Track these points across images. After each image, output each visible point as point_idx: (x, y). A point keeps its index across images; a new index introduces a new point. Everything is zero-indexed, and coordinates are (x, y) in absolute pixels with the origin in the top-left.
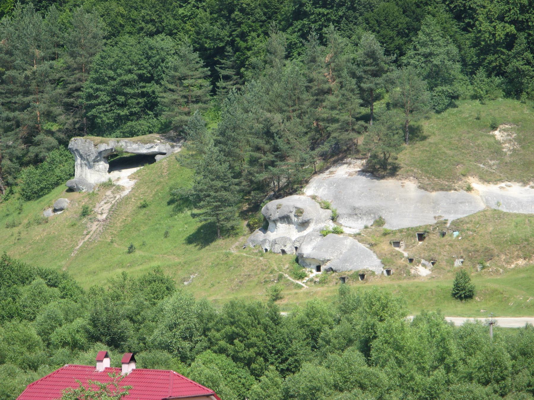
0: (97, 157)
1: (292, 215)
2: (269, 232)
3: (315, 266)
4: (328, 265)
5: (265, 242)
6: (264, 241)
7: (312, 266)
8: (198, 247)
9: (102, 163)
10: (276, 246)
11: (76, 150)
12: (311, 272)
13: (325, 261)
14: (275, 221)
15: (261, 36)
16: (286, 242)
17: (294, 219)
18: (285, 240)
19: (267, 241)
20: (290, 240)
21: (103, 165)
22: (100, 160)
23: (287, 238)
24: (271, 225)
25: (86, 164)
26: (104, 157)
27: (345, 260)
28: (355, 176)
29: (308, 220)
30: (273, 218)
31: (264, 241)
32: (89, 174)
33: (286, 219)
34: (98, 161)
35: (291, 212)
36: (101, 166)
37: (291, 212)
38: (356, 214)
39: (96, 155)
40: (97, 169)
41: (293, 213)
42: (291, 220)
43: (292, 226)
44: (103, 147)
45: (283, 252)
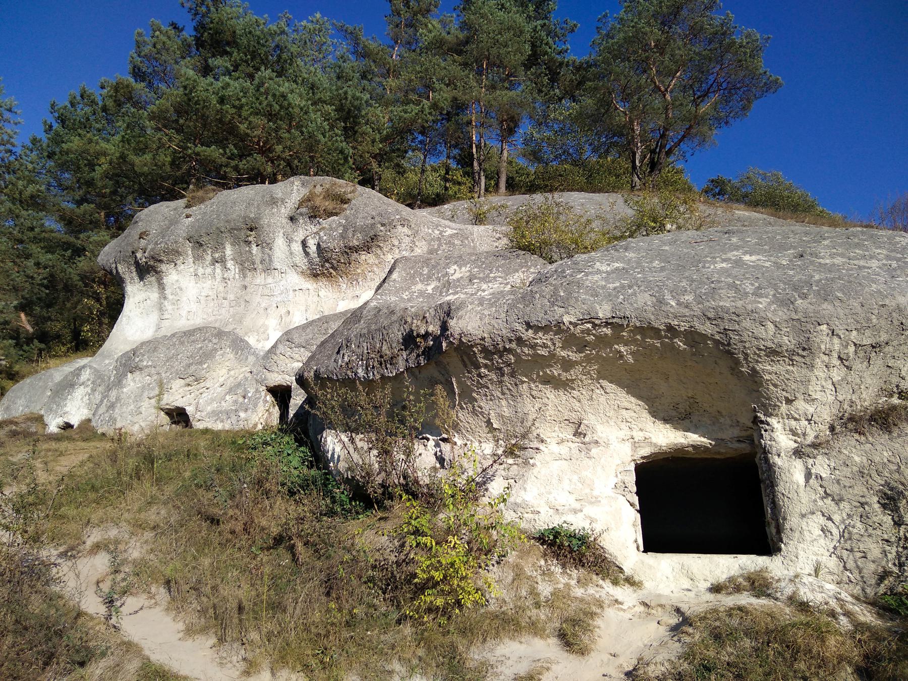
20: (239, 345)
23: (220, 334)
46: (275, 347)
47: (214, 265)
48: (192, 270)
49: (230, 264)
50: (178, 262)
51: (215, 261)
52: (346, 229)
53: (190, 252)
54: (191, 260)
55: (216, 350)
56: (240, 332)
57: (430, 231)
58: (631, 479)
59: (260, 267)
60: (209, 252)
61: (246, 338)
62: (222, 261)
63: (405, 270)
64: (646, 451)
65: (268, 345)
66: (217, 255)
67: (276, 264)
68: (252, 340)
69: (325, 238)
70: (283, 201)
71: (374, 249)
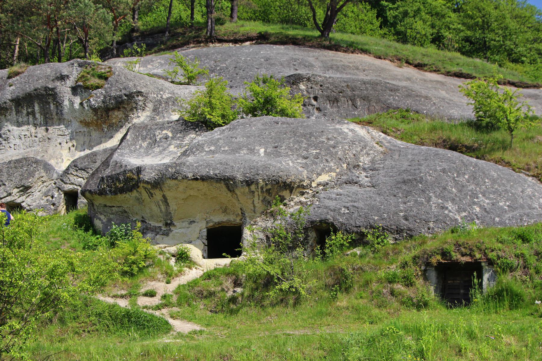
3: (200, 228)
12: (182, 257)
13: (280, 188)
16: (31, 174)
17: (71, 102)
20: (48, 168)
23: (37, 162)
29: (130, 96)
41: (70, 83)
42: (59, 105)
46: (68, 169)
47: (28, 116)
48: (15, 119)
49: (38, 115)
50: (7, 114)
51: (28, 114)
52: (105, 97)
53: (14, 108)
54: (14, 113)
55: (36, 171)
56: (46, 158)
57: (155, 96)
58: (205, 234)
59: (56, 117)
60: (25, 108)
61: (49, 162)
62: (33, 113)
63: (134, 133)
64: (211, 224)
65: (64, 168)
66: (30, 110)
67: (66, 116)
68: (52, 162)
69: (93, 102)
70: (68, 77)
71: (122, 109)
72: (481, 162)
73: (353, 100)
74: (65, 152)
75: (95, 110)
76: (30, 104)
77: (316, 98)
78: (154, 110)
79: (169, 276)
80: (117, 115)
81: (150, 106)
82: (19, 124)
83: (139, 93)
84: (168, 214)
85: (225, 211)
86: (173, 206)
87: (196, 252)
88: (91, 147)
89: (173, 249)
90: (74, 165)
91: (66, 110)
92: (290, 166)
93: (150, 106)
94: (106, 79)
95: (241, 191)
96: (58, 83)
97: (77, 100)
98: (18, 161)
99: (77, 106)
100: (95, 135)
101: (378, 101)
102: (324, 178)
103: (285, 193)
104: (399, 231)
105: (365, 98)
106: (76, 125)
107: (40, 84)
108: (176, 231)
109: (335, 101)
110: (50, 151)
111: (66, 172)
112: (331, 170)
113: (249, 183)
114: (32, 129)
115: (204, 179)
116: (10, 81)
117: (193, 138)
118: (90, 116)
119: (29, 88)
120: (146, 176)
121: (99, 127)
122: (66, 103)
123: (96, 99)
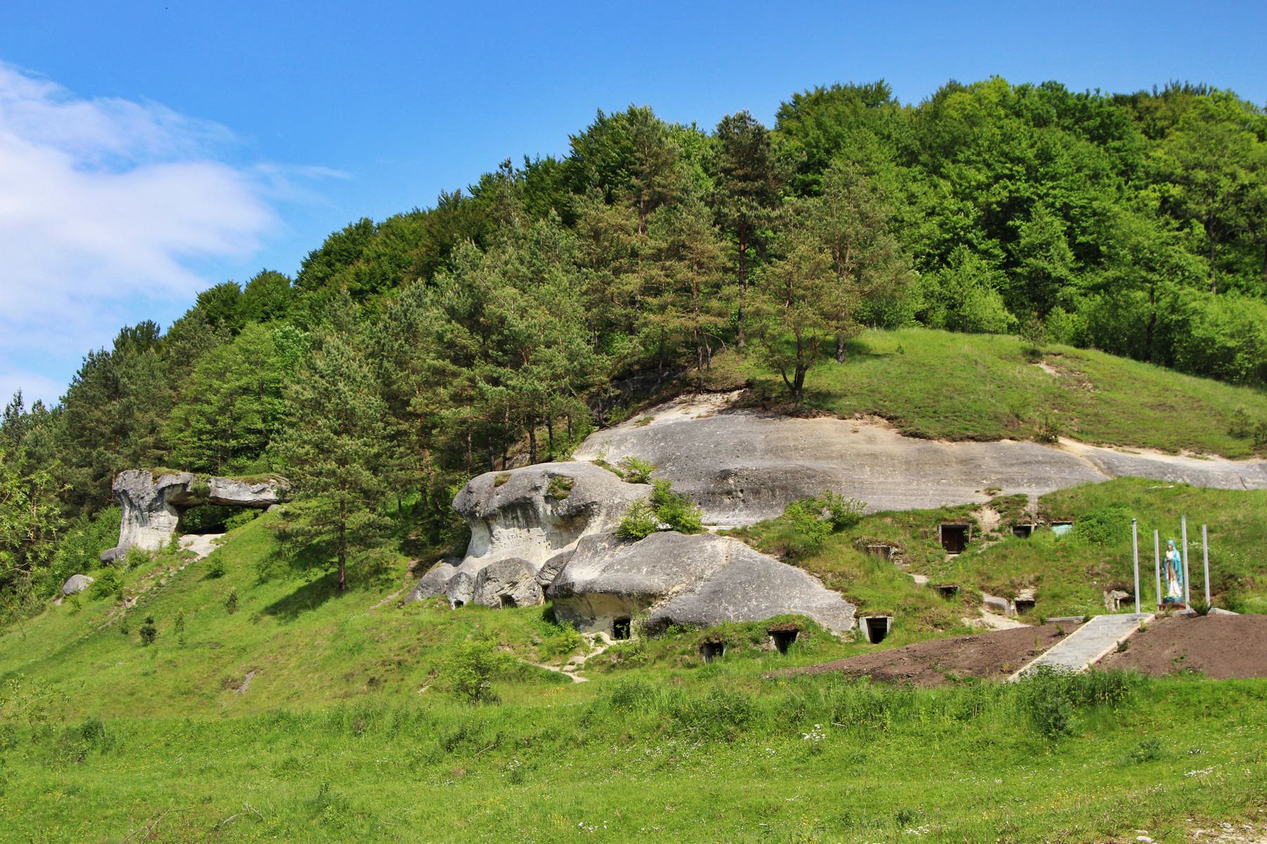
0: (155, 500)
1: (539, 498)
2: (469, 559)
3: (609, 621)
4: (656, 611)
5: (458, 583)
6: (455, 582)
7: (599, 622)
8: (28, 408)
9: (165, 512)
10: (489, 587)
11: (125, 492)
12: (598, 640)
13: (647, 598)
14: (488, 520)
15: (506, 301)
16: (517, 572)
17: (545, 509)
18: (514, 566)
19: (463, 577)
20: (529, 566)
21: (167, 519)
22: (162, 509)
23: (521, 562)
24: (478, 533)
25: (137, 518)
26: (171, 503)
27: (716, 594)
28: (715, 416)
29: (587, 506)
30: (481, 511)
31: (455, 582)
32: (140, 536)
33: (520, 511)
34: (157, 510)
35: (536, 489)
36: (161, 519)
37: (536, 489)
38: (729, 493)
39: (153, 495)
40: (154, 525)
41: (543, 492)
42: (536, 511)
43: (536, 531)
44: (166, 481)
45: (508, 601)
62: (517, 518)
72: (794, 569)
73: (773, 491)
74: (543, 551)
75: (562, 517)
76: (514, 511)
77: (742, 491)
78: (608, 514)
79: (587, 651)
80: (579, 520)
81: (604, 511)
82: (507, 527)
83: (594, 503)
84: (592, 612)
85: (623, 610)
86: (594, 608)
87: (606, 637)
88: (562, 546)
89: (593, 635)
90: (548, 565)
91: (541, 516)
92: (655, 582)
93: (604, 511)
94: (569, 489)
95: (626, 599)
96: (533, 494)
97: (549, 508)
98: (507, 561)
99: (549, 513)
100: (565, 535)
101: (795, 490)
102: (677, 588)
103: (652, 600)
104: (701, 624)
105: (784, 488)
106: (550, 527)
107: (520, 494)
108: (597, 623)
109: (756, 492)
110: (532, 549)
111: (543, 570)
112: (683, 582)
113: (629, 595)
114: (516, 529)
115: (606, 592)
116: (497, 489)
117: (623, 551)
118: (559, 522)
119: (512, 498)
120: (577, 589)
121: (567, 529)
122: (541, 509)
123: (563, 508)
